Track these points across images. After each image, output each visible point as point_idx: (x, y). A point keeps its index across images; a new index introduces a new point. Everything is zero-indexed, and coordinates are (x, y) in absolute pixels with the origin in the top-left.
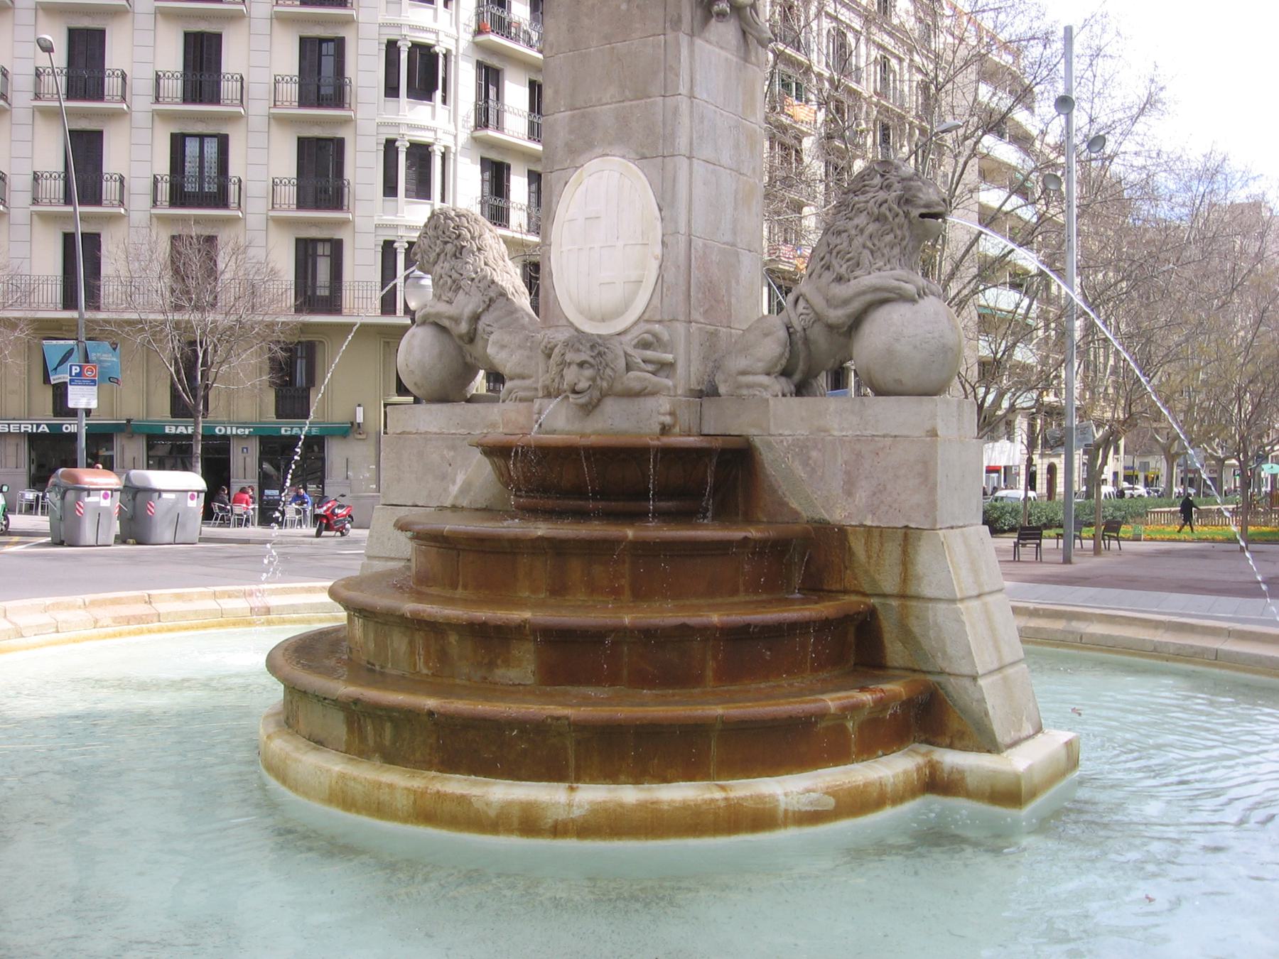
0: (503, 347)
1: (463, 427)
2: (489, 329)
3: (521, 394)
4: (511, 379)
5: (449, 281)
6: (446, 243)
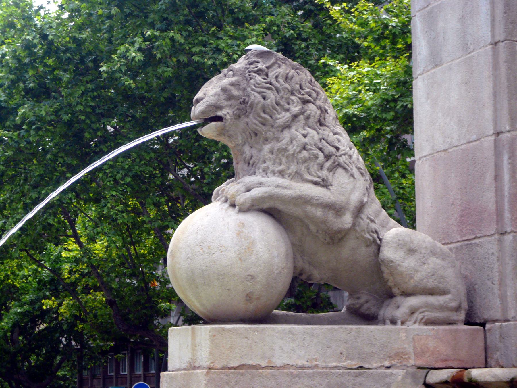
0: (411, 251)
1: (348, 358)
2: (373, 226)
3: (429, 315)
4: (407, 294)
5: (321, 156)
6: (305, 102)
